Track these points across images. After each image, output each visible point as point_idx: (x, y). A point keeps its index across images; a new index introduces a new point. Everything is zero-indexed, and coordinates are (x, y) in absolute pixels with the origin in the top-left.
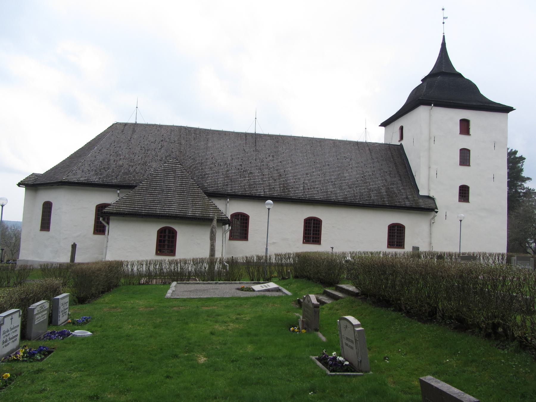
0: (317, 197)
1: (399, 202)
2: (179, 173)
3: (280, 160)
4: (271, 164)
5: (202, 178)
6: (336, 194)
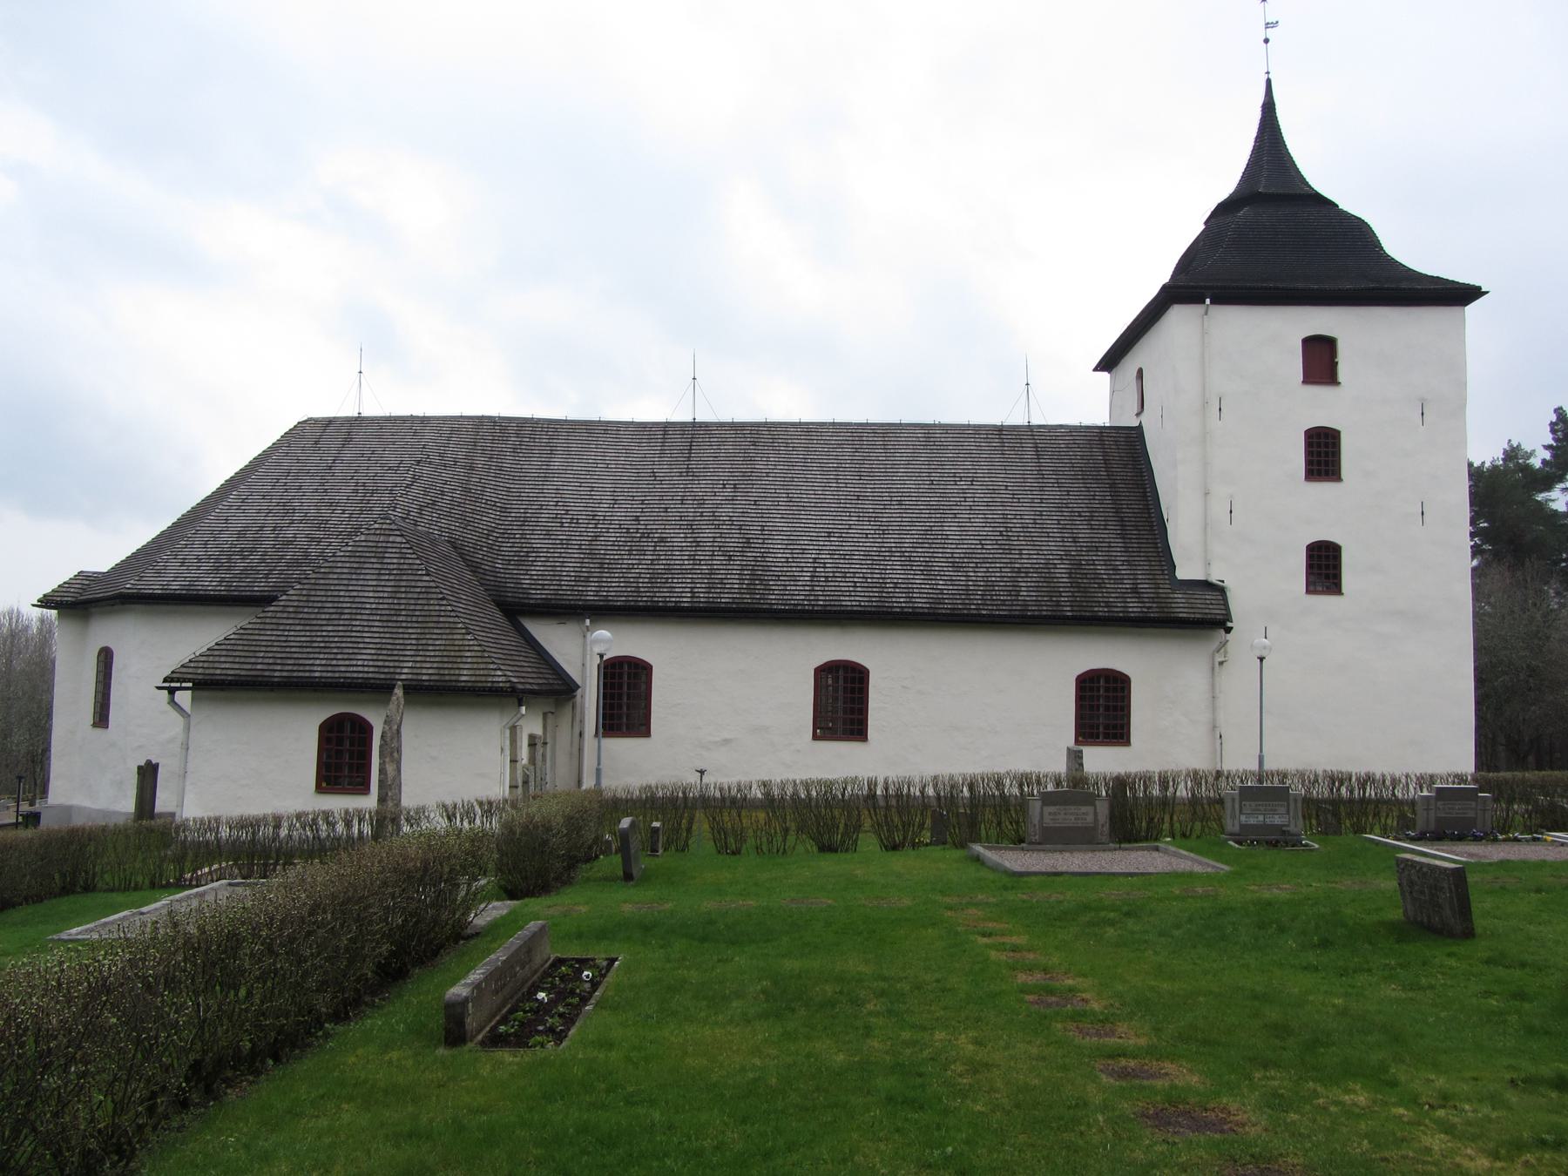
0: (848, 602)
1: (1108, 604)
2: (392, 559)
4: (725, 512)
5: (519, 563)
6: (909, 592)
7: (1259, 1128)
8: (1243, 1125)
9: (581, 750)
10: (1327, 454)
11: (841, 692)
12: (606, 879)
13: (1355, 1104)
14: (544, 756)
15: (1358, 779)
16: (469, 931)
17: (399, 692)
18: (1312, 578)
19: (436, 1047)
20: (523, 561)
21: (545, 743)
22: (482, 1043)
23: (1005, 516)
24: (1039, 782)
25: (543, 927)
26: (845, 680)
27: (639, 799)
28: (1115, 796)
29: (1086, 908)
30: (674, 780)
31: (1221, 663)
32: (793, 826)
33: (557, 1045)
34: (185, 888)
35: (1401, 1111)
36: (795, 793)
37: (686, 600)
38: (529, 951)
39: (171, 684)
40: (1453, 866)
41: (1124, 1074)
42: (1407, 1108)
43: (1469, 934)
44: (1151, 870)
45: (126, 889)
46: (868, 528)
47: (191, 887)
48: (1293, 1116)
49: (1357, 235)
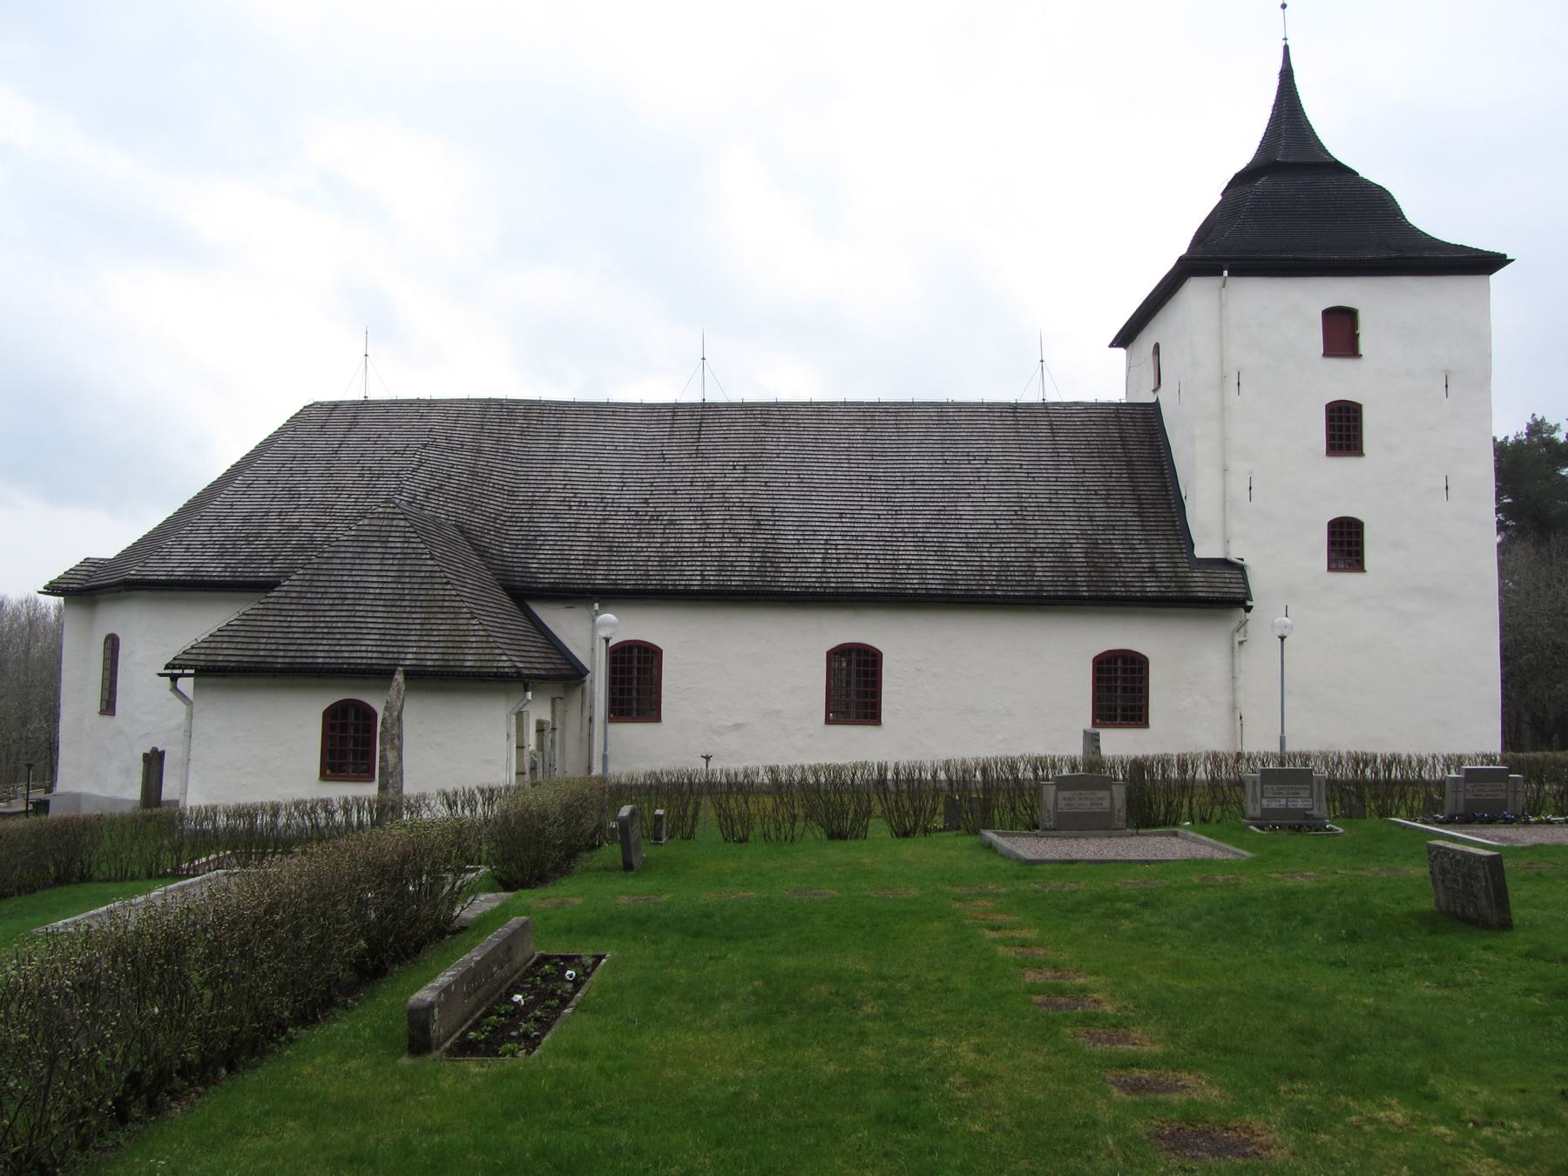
0: (861, 584)
1: (1124, 584)
2: (396, 543)
3: (764, 477)
4: (735, 493)
5: (528, 547)
6: (922, 572)
7: (1286, 1151)
8: (1268, 1148)
9: (590, 736)
10: (1348, 428)
11: (854, 676)
12: (606, 869)
13: (1392, 1122)
14: (553, 742)
15: (1383, 761)
16: (456, 924)
17: (399, 677)
18: (1334, 555)
19: (399, 1056)
20: (531, 545)
21: (554, 729)
22: (450, 1052)
23: (1019, 496)
24: (1054, 766)
25: (525, 925)
26: (858, 664)
27: (643, 785)
28: (1132, 779)
29: (1101, 898)
30: (679, 766)
31: (1241, 643)
32: (800, 812)
33: (529, 1053)
34: (181, 877)
35: (1443, 1129)
36: (804, 779)
37: (696, 583)
38: (510, 948)
39: (174, 670)
40: (1488, 853)
41: (1136, 1087)
42: (1448, 1125)
43: (1506, 925)
44: (1170, 857)
45: (122, 880)
46: (881, 509)
47: (188, 876)
48: (1325, 1138)
49: (1379, 203)
